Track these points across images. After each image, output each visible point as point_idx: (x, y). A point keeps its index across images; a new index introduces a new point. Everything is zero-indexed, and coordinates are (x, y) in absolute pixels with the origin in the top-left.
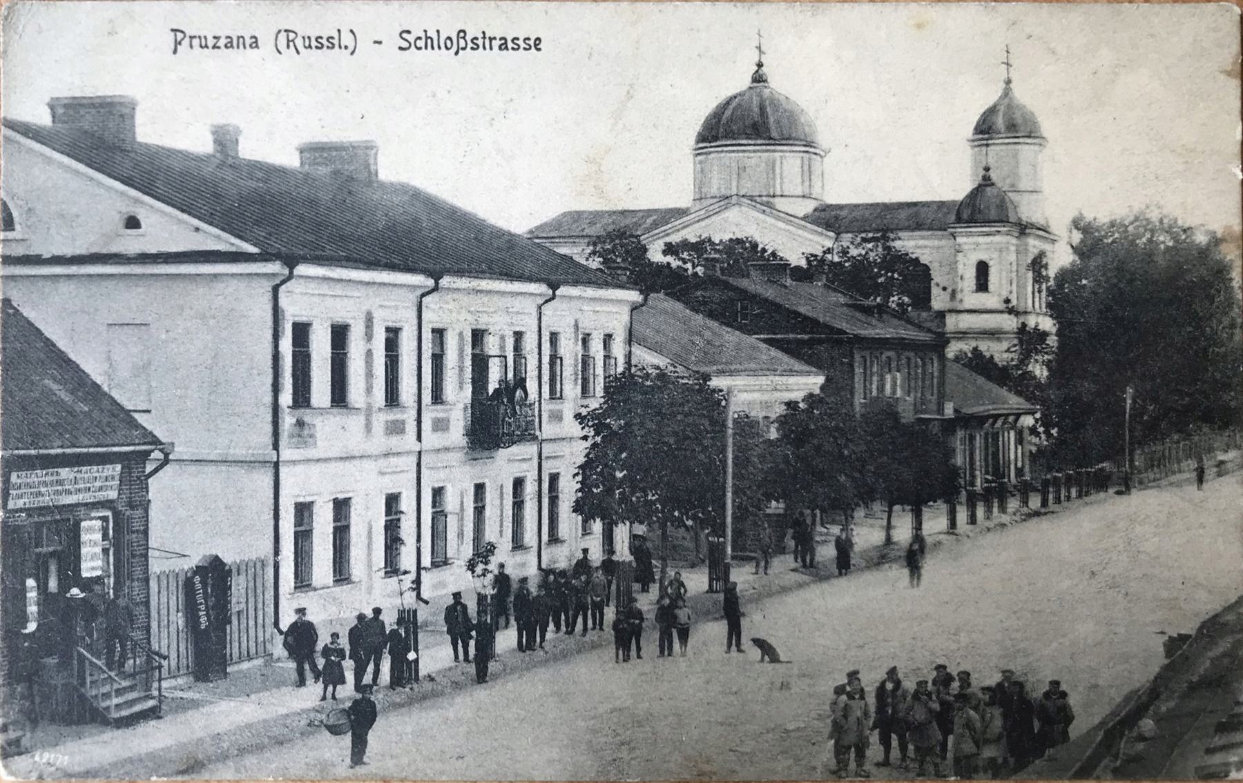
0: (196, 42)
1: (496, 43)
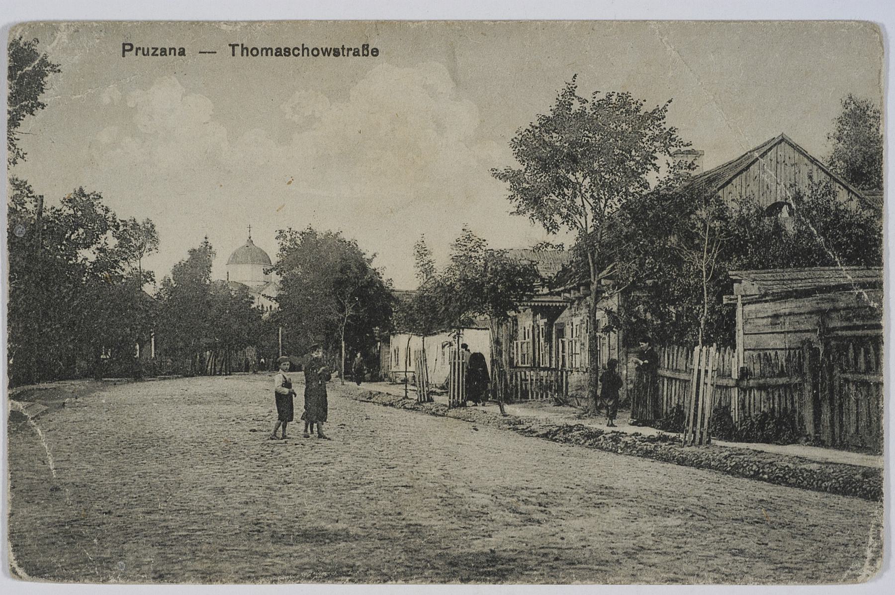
0: (140, 52)
1: (351, 53)
